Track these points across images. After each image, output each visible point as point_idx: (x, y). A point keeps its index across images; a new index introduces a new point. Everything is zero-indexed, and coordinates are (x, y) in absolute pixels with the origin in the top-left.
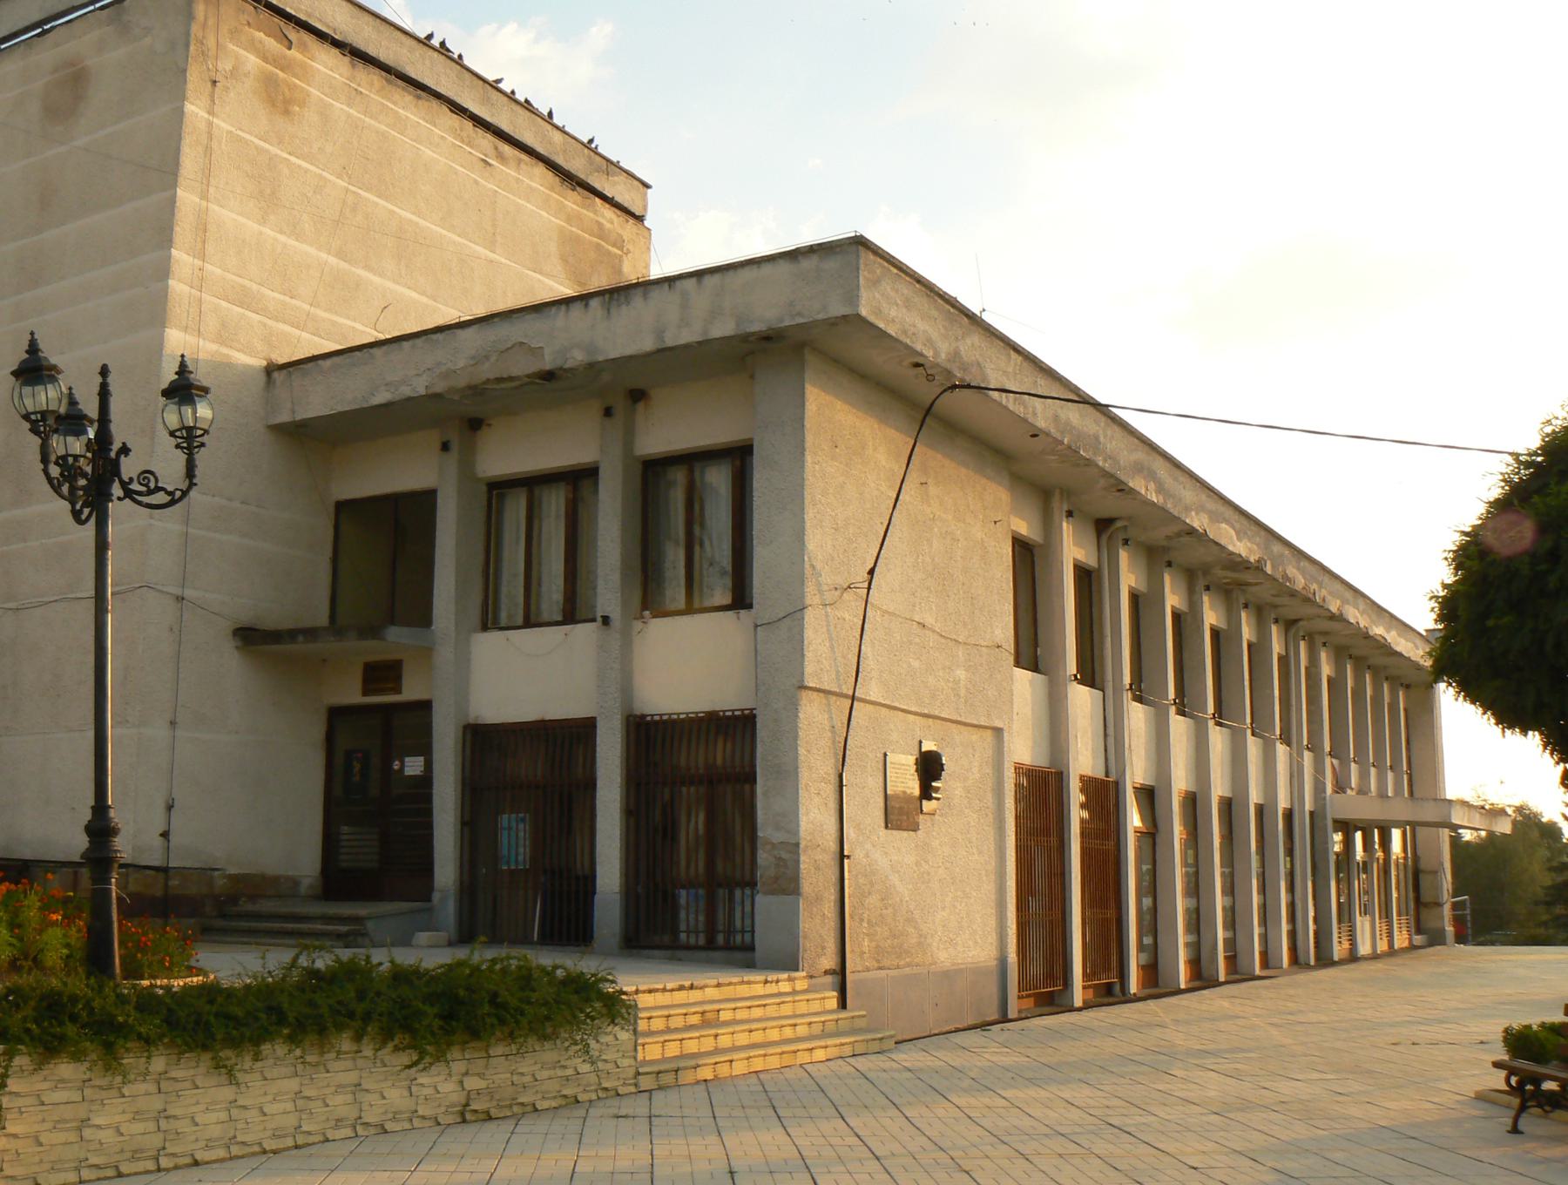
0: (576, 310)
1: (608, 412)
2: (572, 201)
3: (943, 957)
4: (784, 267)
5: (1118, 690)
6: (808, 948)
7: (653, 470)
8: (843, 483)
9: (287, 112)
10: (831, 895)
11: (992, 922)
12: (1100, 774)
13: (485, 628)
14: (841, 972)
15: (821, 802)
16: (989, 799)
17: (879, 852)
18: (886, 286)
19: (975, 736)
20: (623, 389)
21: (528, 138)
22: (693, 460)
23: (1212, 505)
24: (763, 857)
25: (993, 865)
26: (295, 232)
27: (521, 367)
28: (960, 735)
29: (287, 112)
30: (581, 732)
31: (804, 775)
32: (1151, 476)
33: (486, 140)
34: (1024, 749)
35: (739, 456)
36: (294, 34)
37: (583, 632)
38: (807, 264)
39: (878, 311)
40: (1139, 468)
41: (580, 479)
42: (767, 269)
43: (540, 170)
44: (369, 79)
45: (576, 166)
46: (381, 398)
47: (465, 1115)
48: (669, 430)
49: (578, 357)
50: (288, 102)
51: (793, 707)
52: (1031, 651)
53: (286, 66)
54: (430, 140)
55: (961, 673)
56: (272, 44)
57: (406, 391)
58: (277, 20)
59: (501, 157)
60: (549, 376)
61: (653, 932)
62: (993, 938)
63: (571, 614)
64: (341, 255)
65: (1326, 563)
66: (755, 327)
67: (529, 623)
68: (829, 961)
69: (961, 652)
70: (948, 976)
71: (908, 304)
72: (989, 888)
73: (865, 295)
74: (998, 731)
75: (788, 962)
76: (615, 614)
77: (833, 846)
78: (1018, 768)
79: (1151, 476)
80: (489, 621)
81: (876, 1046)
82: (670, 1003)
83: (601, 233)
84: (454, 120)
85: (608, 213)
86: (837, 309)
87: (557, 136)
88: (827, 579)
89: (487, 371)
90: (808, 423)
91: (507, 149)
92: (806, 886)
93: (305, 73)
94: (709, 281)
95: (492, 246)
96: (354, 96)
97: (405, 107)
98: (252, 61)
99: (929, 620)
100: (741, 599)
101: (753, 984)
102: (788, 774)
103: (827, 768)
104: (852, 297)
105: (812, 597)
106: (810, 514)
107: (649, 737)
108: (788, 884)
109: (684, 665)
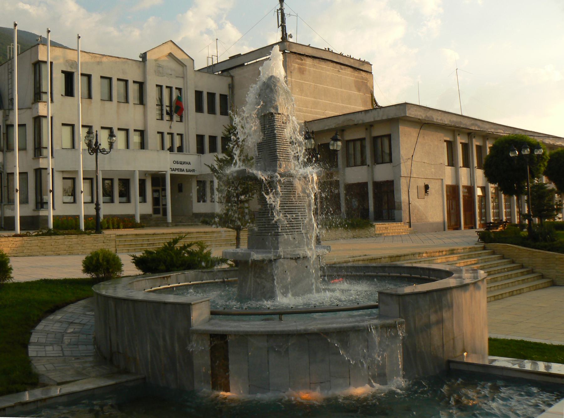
0: (360, 113)
1: (367, 129)
2: (356, 74)
3: (431, 220)
4: (394, 107)
5: (473, 168)
6: (403, 218)
7: (375, 139)
8: (407, 142)
9: (303, 73)
10: (408, 210)
11: (442, 214)
12: (469, 185)
13: (347, 166)
14: (410, 223)
15: (407, 195)
16: (440, 192)
17: (418, 203)
18: (412, 109)
19: (437, 181)
20: (370, 126)
21: (347, 63)
22: (382, 137)
23: (495, 127)
24: (396, 204)
25: (441, 204)
26: (307, 96)
27: (351, 123)
28: (433, 181)
29: (303, 73)
30: (365, 184)
31: (402, 191)
32: (476, 125)
33: (338, 66)
34: (449, 181)
35: (389, 136)
36: (302, 57)
37: (365, 167)
38: (398, 107)
39: (410, 114)
40: (473, 125)
41: (362, 140)
42: (391, 108)
43: (349, 69)
44: (317, 61)
45: (356, 66)
46: (326, 128)
47: (354, 237)
48: (377, 132)
49: (361, 122)
50: (303, 71)
51: (400, 180)
52: (452, 162)
53: (302, 64)
54: (328, 70)
55: (433, 170)
56: (299, 61)
57: (331, 127)
58: (300, 56)
59: (342, 69)
60: (356, 125)
61: (379, 218)
62: (442, 217)
63: (363, 163)
64: (314, 98)
65: (533, 130)
66: (390, 117)
67: (355, 166)
68: (408, 221)
69: (433, 166)
70: (432, 224)
71: (416, 110)
72: (441, 208)
73: (407, 112)
74: (442, 180)
75: (400, 221)
76: (370, 165)
77: (408, 202)
78: (447, 186)
79: (476, 125)
80: (348, 165)
81: (503, 270)
82: (379, 227)
83: (363, 78)
84: (332, 64)
85: (364, 74)
86: (403, 115)
87: (352, 60)
88: (405, 158)
89: (345, 124)
90: (400, 133)
91: (343, 67)
92: (403, 209)
93: (305, 65)
94: (382, 109)
95: (341, 87)
96: (314, 66)
97: (323, 65)
98: (296, 66)
99: (426, 161)
100: (391, 161)
101: (394, 224)
102: (399, 191)
103: (406, 189)
104: (406, 113)
105: (402, 161)
106: (401, 148)
107: (377, 185)
108: (400, 208)
109: (382, 173)
